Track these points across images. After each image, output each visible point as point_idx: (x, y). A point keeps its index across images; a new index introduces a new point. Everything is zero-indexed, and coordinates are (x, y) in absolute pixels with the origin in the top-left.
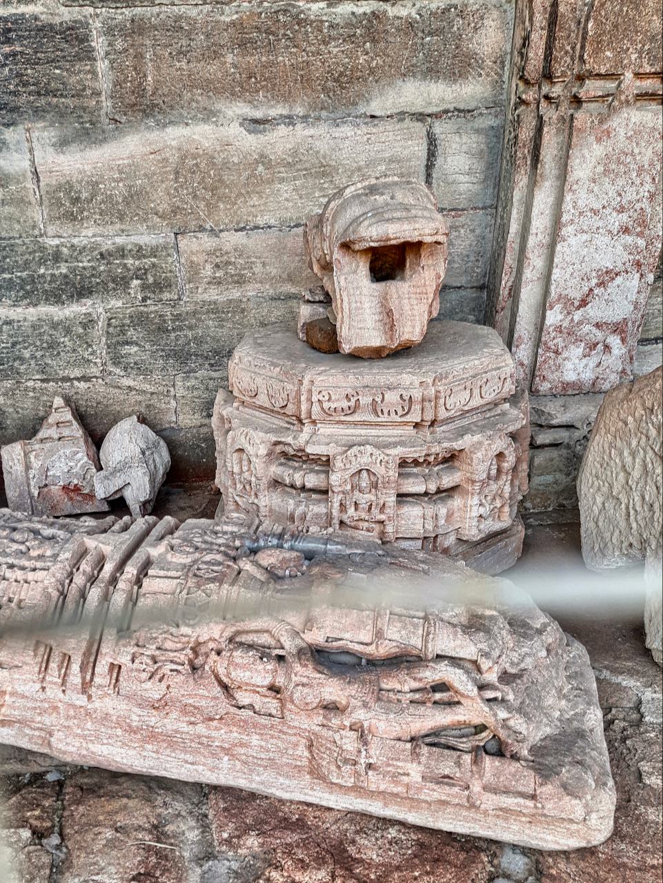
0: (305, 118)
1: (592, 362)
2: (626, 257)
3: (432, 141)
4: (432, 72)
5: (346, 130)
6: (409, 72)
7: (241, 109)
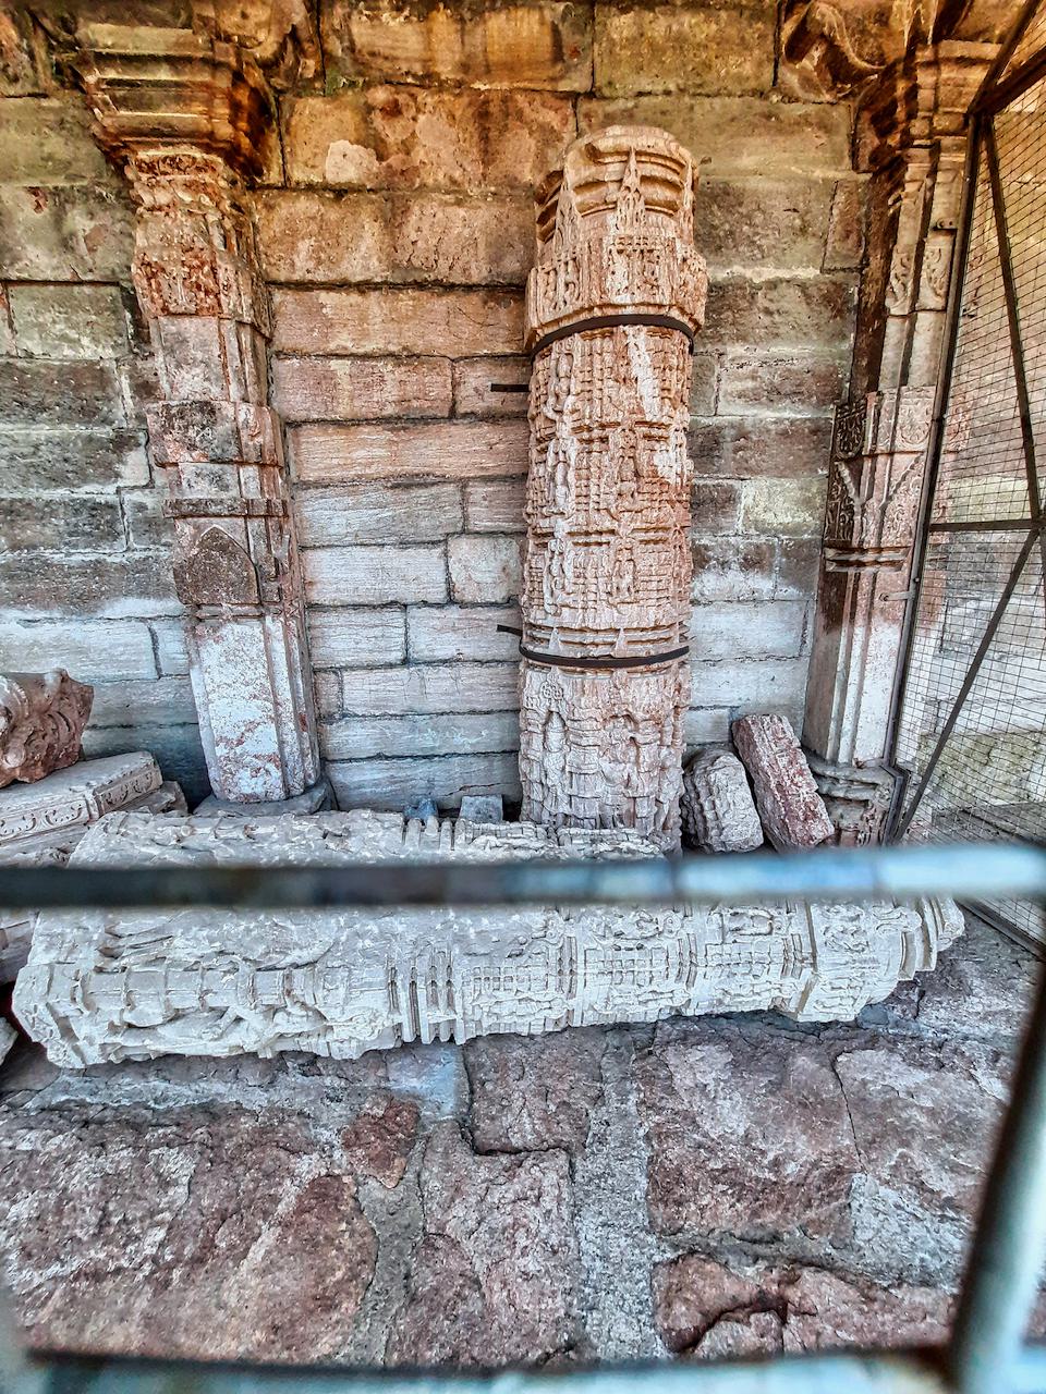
0: (62, 619)
1: (260, 781)
2: (261, 714)
3: (153, 635)
4: (144, 593)
5: (91, 626)
6: (128, 594)
7: (14, 613)
